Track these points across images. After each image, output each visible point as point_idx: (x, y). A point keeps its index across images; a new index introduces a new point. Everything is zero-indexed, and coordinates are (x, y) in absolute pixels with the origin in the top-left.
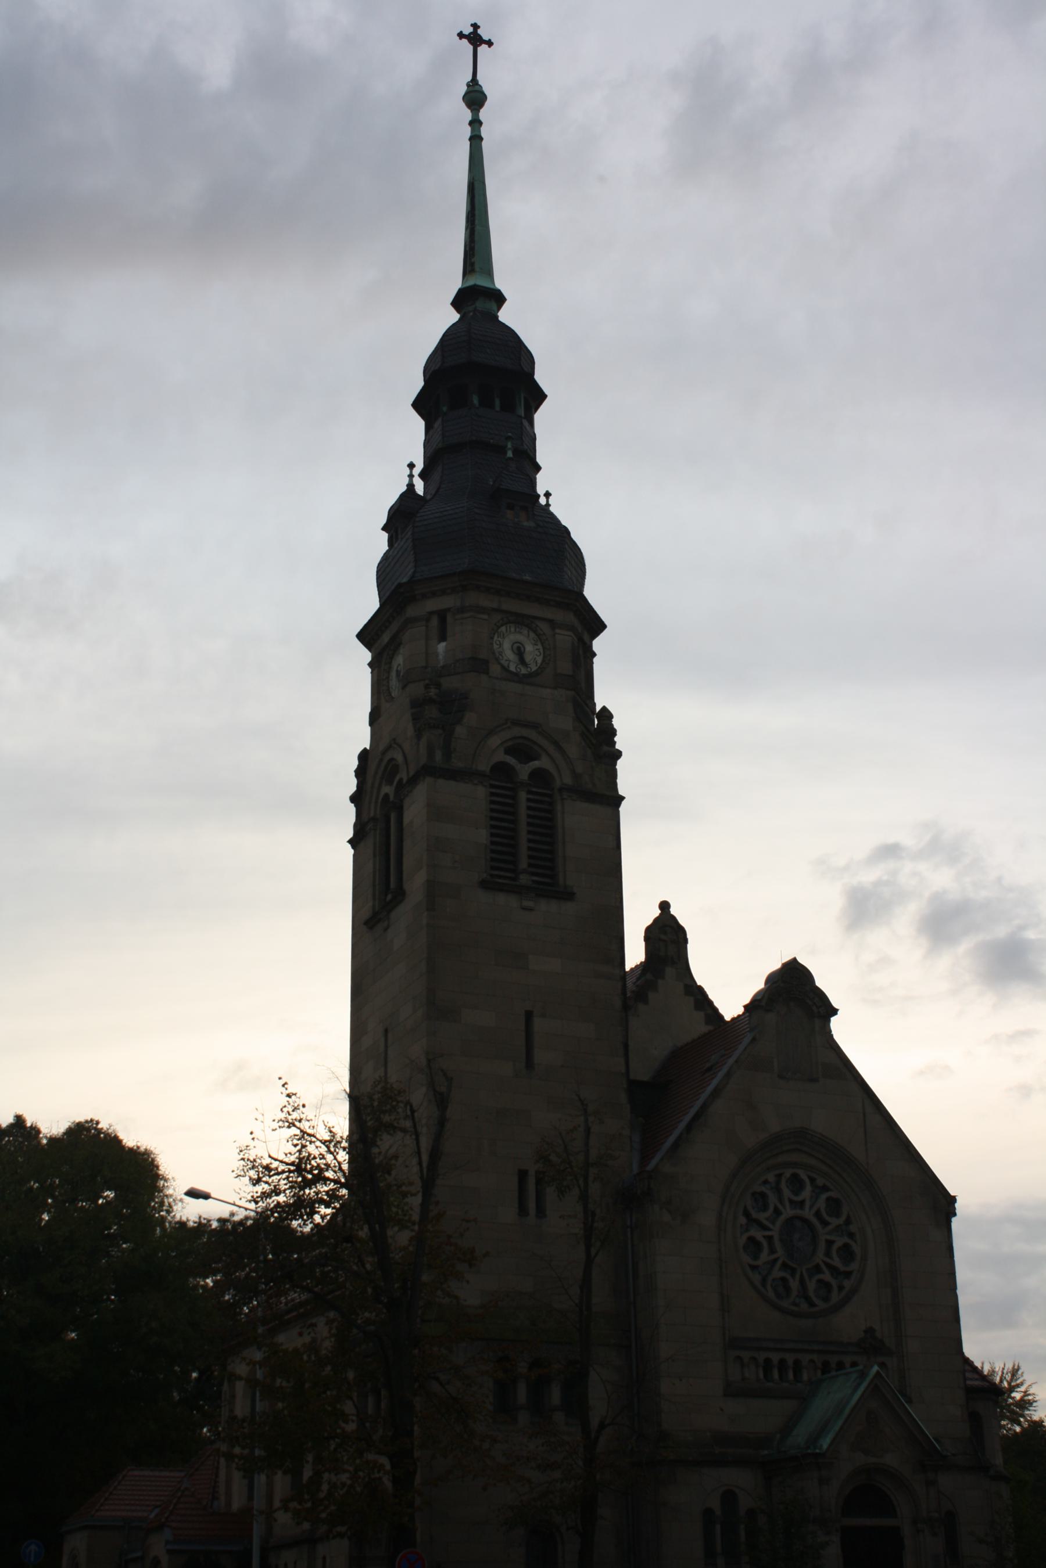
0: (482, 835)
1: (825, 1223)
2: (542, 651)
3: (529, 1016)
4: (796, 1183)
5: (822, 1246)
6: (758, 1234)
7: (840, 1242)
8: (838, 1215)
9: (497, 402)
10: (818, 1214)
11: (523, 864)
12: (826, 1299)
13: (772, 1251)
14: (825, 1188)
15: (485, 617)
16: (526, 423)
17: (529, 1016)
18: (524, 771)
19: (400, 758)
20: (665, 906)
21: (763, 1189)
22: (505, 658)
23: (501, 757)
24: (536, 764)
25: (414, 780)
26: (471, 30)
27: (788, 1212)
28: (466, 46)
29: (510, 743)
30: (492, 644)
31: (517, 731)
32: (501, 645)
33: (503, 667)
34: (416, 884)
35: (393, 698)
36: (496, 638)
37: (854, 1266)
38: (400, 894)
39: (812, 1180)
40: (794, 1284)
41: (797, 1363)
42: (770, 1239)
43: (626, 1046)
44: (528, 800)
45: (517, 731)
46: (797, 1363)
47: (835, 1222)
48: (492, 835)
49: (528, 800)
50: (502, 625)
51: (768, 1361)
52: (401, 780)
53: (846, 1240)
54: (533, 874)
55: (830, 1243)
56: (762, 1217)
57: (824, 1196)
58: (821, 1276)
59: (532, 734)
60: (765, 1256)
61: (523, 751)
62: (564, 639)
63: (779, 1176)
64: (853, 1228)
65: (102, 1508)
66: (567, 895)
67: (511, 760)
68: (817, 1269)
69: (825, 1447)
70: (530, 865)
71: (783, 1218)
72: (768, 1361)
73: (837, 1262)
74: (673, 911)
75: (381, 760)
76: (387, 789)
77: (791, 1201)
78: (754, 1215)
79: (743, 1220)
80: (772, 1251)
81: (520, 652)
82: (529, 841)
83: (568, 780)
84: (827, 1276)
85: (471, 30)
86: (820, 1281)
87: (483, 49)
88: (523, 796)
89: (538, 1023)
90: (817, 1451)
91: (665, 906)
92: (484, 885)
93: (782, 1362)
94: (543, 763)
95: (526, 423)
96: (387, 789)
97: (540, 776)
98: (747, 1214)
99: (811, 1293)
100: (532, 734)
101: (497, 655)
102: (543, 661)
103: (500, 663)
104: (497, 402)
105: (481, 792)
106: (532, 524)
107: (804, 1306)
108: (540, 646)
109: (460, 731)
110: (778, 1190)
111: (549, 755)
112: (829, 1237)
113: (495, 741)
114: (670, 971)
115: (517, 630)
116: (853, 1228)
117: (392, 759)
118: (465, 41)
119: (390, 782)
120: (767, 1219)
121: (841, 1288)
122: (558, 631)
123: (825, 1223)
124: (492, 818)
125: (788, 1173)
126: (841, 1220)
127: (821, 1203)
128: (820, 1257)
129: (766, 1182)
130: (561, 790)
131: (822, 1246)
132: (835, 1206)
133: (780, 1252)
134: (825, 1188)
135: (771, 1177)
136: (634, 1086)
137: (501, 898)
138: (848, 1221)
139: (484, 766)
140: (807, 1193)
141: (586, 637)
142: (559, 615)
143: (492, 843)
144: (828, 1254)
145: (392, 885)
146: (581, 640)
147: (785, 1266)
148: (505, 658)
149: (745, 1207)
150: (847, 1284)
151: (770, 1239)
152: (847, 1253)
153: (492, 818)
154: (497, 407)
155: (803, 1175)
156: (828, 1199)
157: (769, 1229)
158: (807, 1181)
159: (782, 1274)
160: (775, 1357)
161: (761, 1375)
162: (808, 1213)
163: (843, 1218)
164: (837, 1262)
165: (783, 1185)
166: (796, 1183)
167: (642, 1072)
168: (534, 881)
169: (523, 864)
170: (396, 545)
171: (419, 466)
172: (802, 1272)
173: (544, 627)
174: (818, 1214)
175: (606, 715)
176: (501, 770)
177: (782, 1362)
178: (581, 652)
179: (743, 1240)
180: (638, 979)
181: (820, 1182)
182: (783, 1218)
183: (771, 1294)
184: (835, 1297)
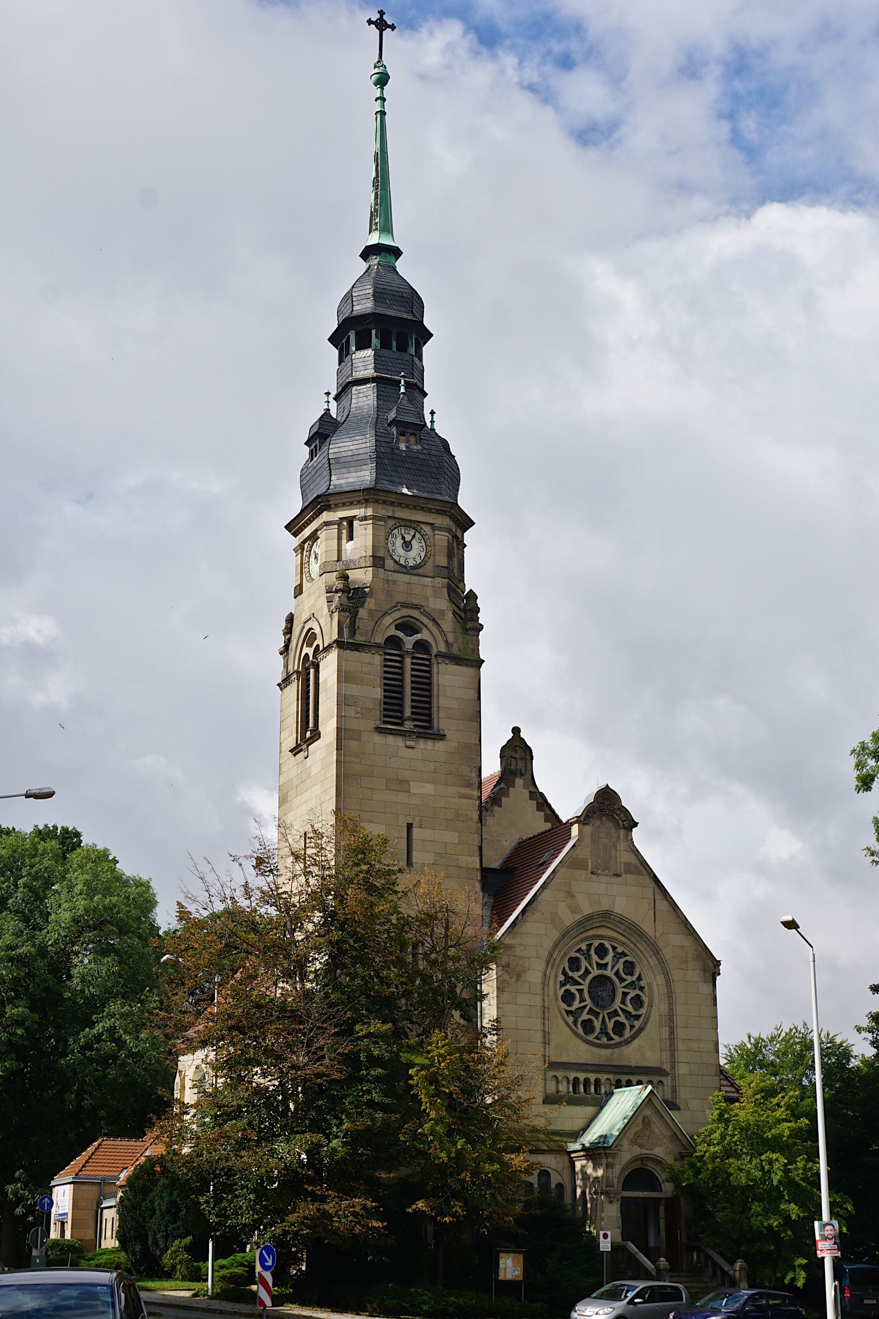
0: (378, 693)
1: (622, 980)
2: (424, 547)
3: (410, 827)
4: (602, 951)
5: (619, 996)
6: (573, 989)
7: (633, 993)
8: (632, 974)
9: (394, 344)
10: (617, 973)
11: (408, 713)
12: (621, 1035)
13: (582, 1000)
14: (624, 954)
15: (383, 523)
16: (416, 360)
17: (410, 827)
18: (409, 642)
19: (317, 631)
20: (516, 731)
21: (577, 955)
22: (397, 554)
23: (393, 632)
24: (418, 636)
25: (327, 649)
26: (378, 16)
27: (595, 972)
28: (374, 30)
29: (400, 621)
30: (387, 544)
31: (405, 612)
32: (394, 544)
33: (395, 561)
34: (328, 726)
35: (313, 580)
36: (390, 539)
37: (643, 1011)
38: (316, 735)
39: (614, 948)
40: (597, 1024)
41: (597, 1081)
42: (580, 991)
43: (481, 848)
44: (412, 664)
45: (405, 612)
46: (597, 1081)
47: (629, 979)
48: (385, 691)
49: (412, 676)
50: (395, 528)
51: (576, 1080)
52: (318, 646)
53: (638, 992)
54: (414, 720)
55: (625, 994)
56: (576, 975)
57: (622, 961)
58: (617, 1018)
59: (415, 613)
60: (576, 1004)
61: (408, 627)
62: (442, 538)
63: (590, 945)
64: (642, 983)
65: (84, 1169)
66: (441, 737)
67: (400, 634)
68: (615, 1013)
69: (611, 1143)
70: (412, 713)
71: (591, 976)
72: (576, 1080)
73: (630, 1008)
74: (523, 735)
75: (304, 627)
76: (306, 650)
77: (597, 964)
78: (570, 974)
79: (562, 978)
80: (582, 1000)
81: (407, 545)
82: (412, 670)
83: (443, 648)
84: (622, 1019)
85: (379, 101)
86: (616, 1022)
87: (387, 32)
88: (408, 661)
89: (416, 832)
90: (605, 1145)
91: (516, 731)
92: (379, 730)
93: (587, 1080)
94: (424, 635)
95: (416, 360)
96: (306, 650)
97: (421, 646)
98: (564, 973)
99: (610, 1031)
100: (415, 613)
101: (391, 551)
102: (425, 556)
103: (393, 559)
104: (394, 344)
105: (377, 659)
106: (419, 447)
107: (604, 1040)
108: (423, 544)
109: (362, 613)
110: (588, 957)
111: (427, 628)
112: (624, 990)
113: (388, 620)
114: (519, 782)
115: (407, 531)
116: (642, 983)
117: (311, 629)
118: (373, 26)
119: (310, 645)
120: (579, 977)
121: (632, 1027)
122: (436, 532)
123: (622, 980)
124: (385, 678)
125: (596, 943)
126: (634, 978)
127: (620, 965)
128: (617, 1004)
129: (579, 950)
130: (436, 656)
131: (619, 996)
132: (630, 967)
133: (588, 1001)
134: (624, 954)
135: (584, 947)
136: (486, 872)
137: (391, 739)
138: (639, 978)
139: (380, 639)
140: (609, 959)
141: (459, 534)
142: (439, 520)
143: (385, 697)
144: (623, 1002)
145: (311, 725)
146: (455, 537)
147: (591, 1011)
148: (397, 554)
149: (564, 968)
150: (637, 1024)
151: (580, 991)
152: (637, 1001)
153: (385, 678)
154: (394, 349)
155: (607, 944)
156: (625, 962)
157: (581, 984)
158: (611, 949)
159: (589, 1017)
160: (582, 1076)
161: (571, 1089)
162: (609, 972)
163: (636, 975)
164: (630, 1008)
165: (592, 952)
166: (602, 951)
167: (494, 862)
168: (415, 726)
169: (408, 713)
170: (315, 459)
171: (334, 393)
172: (604, 1016)
173: (427, 529)
174: (617, 973)
175: (472, 596)
176: (393, 642)
177: (587, 1080)
178: (455, 545)
179: (561, 992)
180: (495, 787)
181: (620, 949)
182: (591, 976)
183: (580, 1031)
184: (627, 1033)
